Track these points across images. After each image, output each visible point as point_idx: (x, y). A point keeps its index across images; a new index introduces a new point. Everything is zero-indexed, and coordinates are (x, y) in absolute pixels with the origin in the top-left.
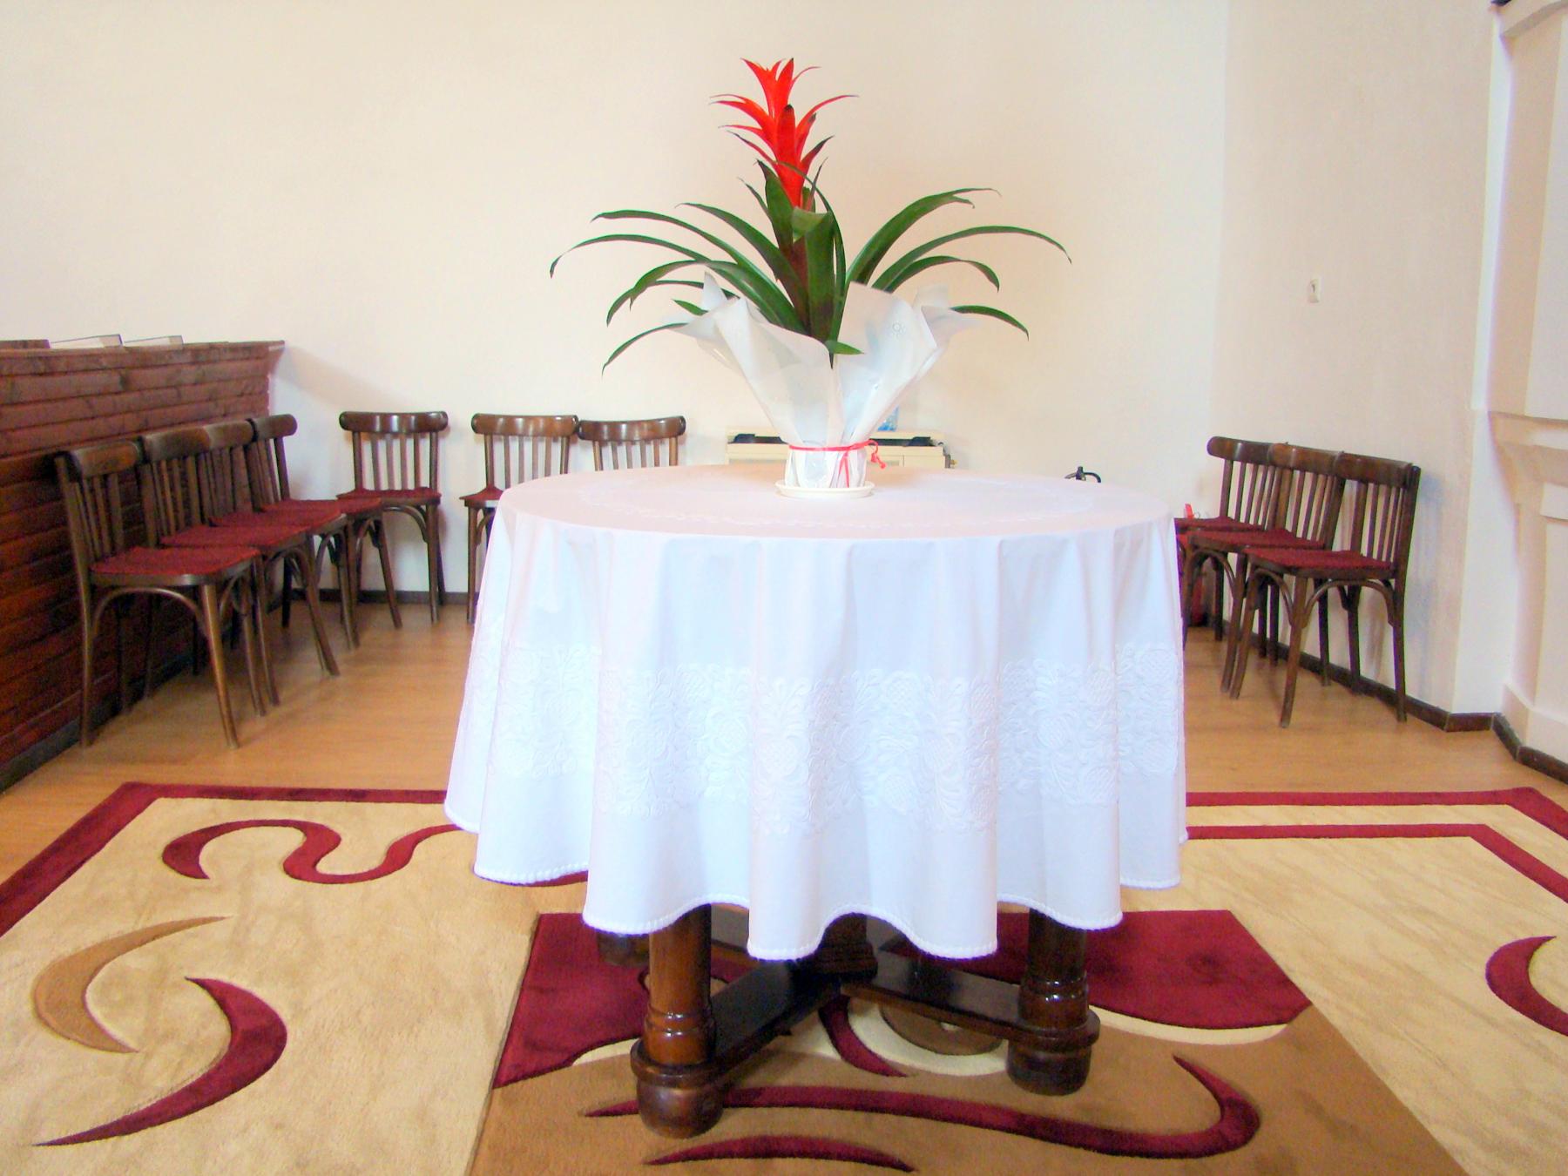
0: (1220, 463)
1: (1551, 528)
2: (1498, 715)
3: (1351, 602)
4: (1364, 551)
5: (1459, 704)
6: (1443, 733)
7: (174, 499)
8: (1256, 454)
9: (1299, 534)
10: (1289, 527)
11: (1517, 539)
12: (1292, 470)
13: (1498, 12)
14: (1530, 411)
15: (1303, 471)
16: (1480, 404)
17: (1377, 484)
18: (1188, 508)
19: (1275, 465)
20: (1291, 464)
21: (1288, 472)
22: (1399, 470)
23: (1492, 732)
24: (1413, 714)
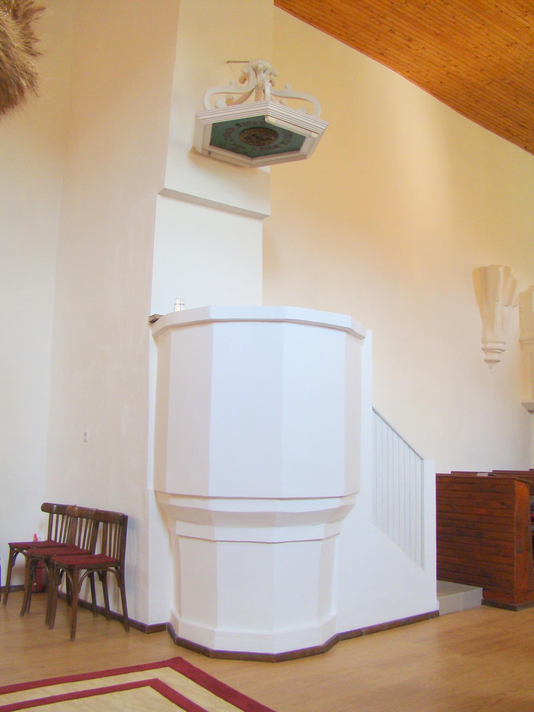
1: (181, 540)
2: (169, 623)
3: (103, 578)
4: (108, 554)
5: (151, 621)
6: (146, 635)
7: (396, 25)
8: (62, 510)
9: (81, 547)
10: (76, 544)
11: (171, 544)
12: (77, 517)
14: (168, 491)
15: (82, 518)
16: (151, 487)
17: (111, 523)
18: (35, 536)
21: (75, 519)
23: (167, 631)
24: (132, 626)
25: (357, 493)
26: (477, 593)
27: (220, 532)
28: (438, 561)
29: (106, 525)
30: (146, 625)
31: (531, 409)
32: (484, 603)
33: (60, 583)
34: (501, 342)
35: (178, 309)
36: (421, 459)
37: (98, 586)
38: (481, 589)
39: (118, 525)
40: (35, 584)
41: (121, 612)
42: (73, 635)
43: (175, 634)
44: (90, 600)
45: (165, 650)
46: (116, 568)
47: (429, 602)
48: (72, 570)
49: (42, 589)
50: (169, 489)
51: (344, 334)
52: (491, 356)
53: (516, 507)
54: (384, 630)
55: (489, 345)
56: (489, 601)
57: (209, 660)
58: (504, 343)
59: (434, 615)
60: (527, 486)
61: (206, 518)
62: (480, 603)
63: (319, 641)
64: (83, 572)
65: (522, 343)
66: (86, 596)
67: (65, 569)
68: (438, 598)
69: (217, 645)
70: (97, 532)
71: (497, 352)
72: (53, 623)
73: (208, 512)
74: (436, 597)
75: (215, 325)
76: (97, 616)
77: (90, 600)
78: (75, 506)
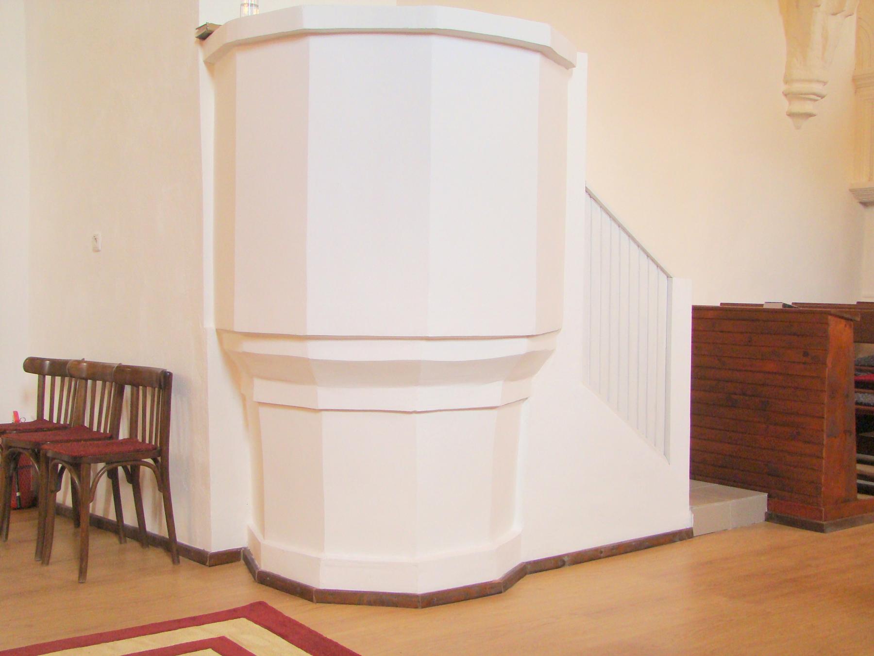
0: (35, 377)
1: (264, 411)
2: (245, 548)
3: (133, 478)
4: (140, 438)
5: (216, 545)
8: (59, 368)
9: (95, 429)
10: (87, 424)
11: (246, 418)
12: (86, 380)
13: (202, 45)
14: (237, 328)
15: (94, 380)
16: (210, 324)
17: (145, 387)
18: (16, 414)
19: (72, 376)
20: (84, 376)
21: (84, 381)
22: (157, 373)
23: (242, 562)
25: (557, 331)
26: (758, 501)
27: (326, 396)
28: (692, 449)
29: (135, 388)
30: (207, 553)
31: (865, 200)
32: (769, 518)
33: (58, 488)
34: (818, 81)
35: (246, 10)
36: (668, 277)
37: (126, 491)
38: (764, 496)
39: (157, 389)
40: (18, 494)
41: (165, 534)
42: (83, 572)
43: (256, 566)
44: (112, 516)
45: (239, 590)
46: (155, 460)
47: (680, 516)
48: (77, 465)
49: (31, 503)
50: (241, 325)
51: (537, 58)
52: (800, 104)
53: (829, 360)
54: (600, 558)
55: (797, 87)
56: (777, 516)
57: (311, 605)
58: (825, 83)
59: (684, 535)
60: (850, 326)
61: (302, 372)
62: (764, 517)
63: (494, 574)
64: (101, 466)
65: (858, 83)
66: (106, 510)
67: (65, 465)
68: (691, 508)
69: (325, 581)
70: (122, 398)
71: (811, 100)
72: (49, 557)
73: (305, 362)
74: (688, 507)
75: (313, 41)
76: (126, 542)
77: (112, 516)
78: (83, 361)
